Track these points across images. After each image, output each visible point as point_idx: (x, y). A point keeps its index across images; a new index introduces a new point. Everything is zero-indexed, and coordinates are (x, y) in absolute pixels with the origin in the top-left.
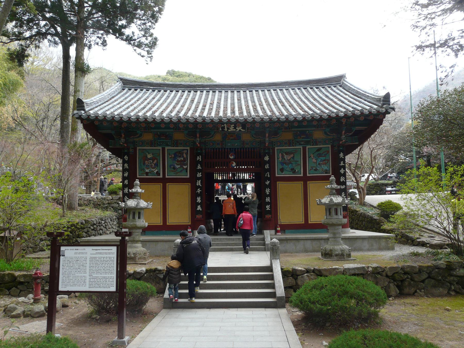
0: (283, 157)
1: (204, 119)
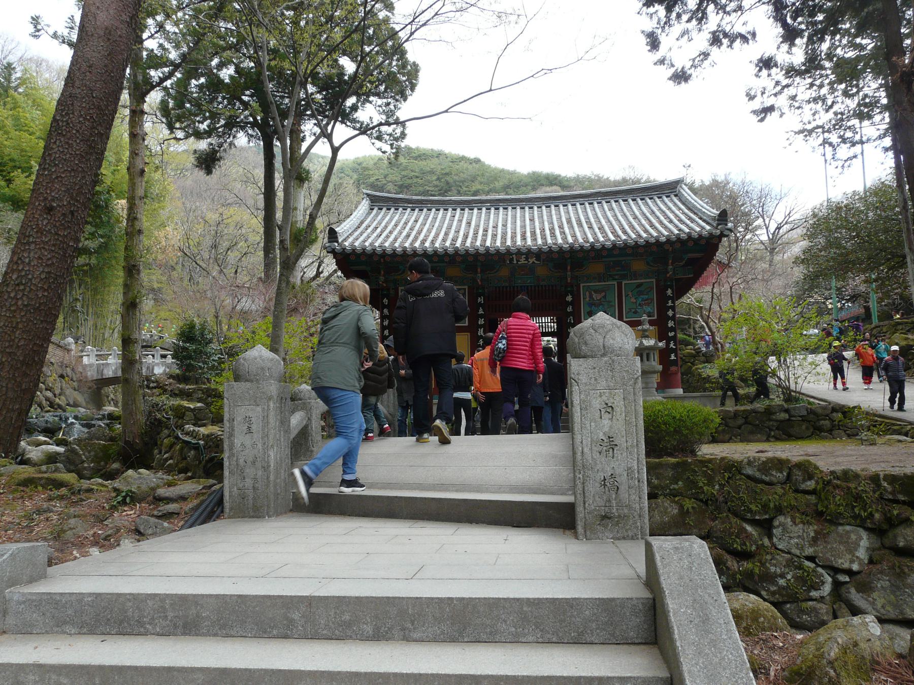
0: (591, 296)
1: (487, 249)
